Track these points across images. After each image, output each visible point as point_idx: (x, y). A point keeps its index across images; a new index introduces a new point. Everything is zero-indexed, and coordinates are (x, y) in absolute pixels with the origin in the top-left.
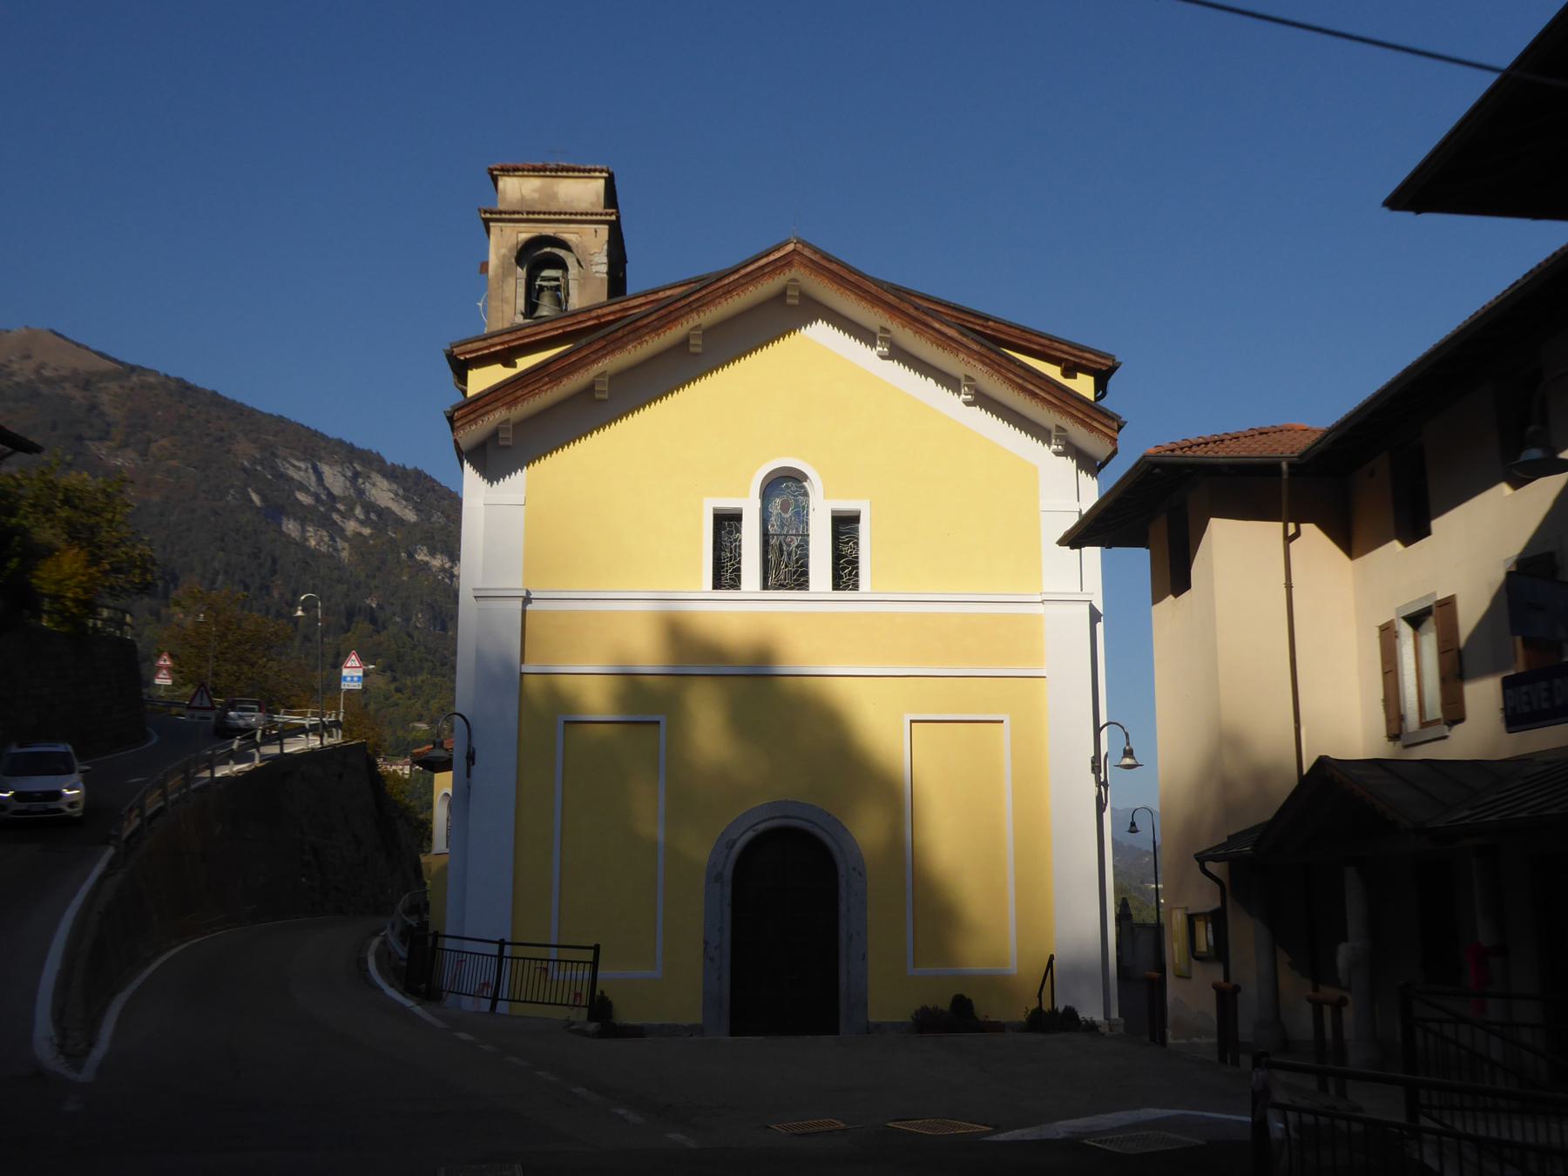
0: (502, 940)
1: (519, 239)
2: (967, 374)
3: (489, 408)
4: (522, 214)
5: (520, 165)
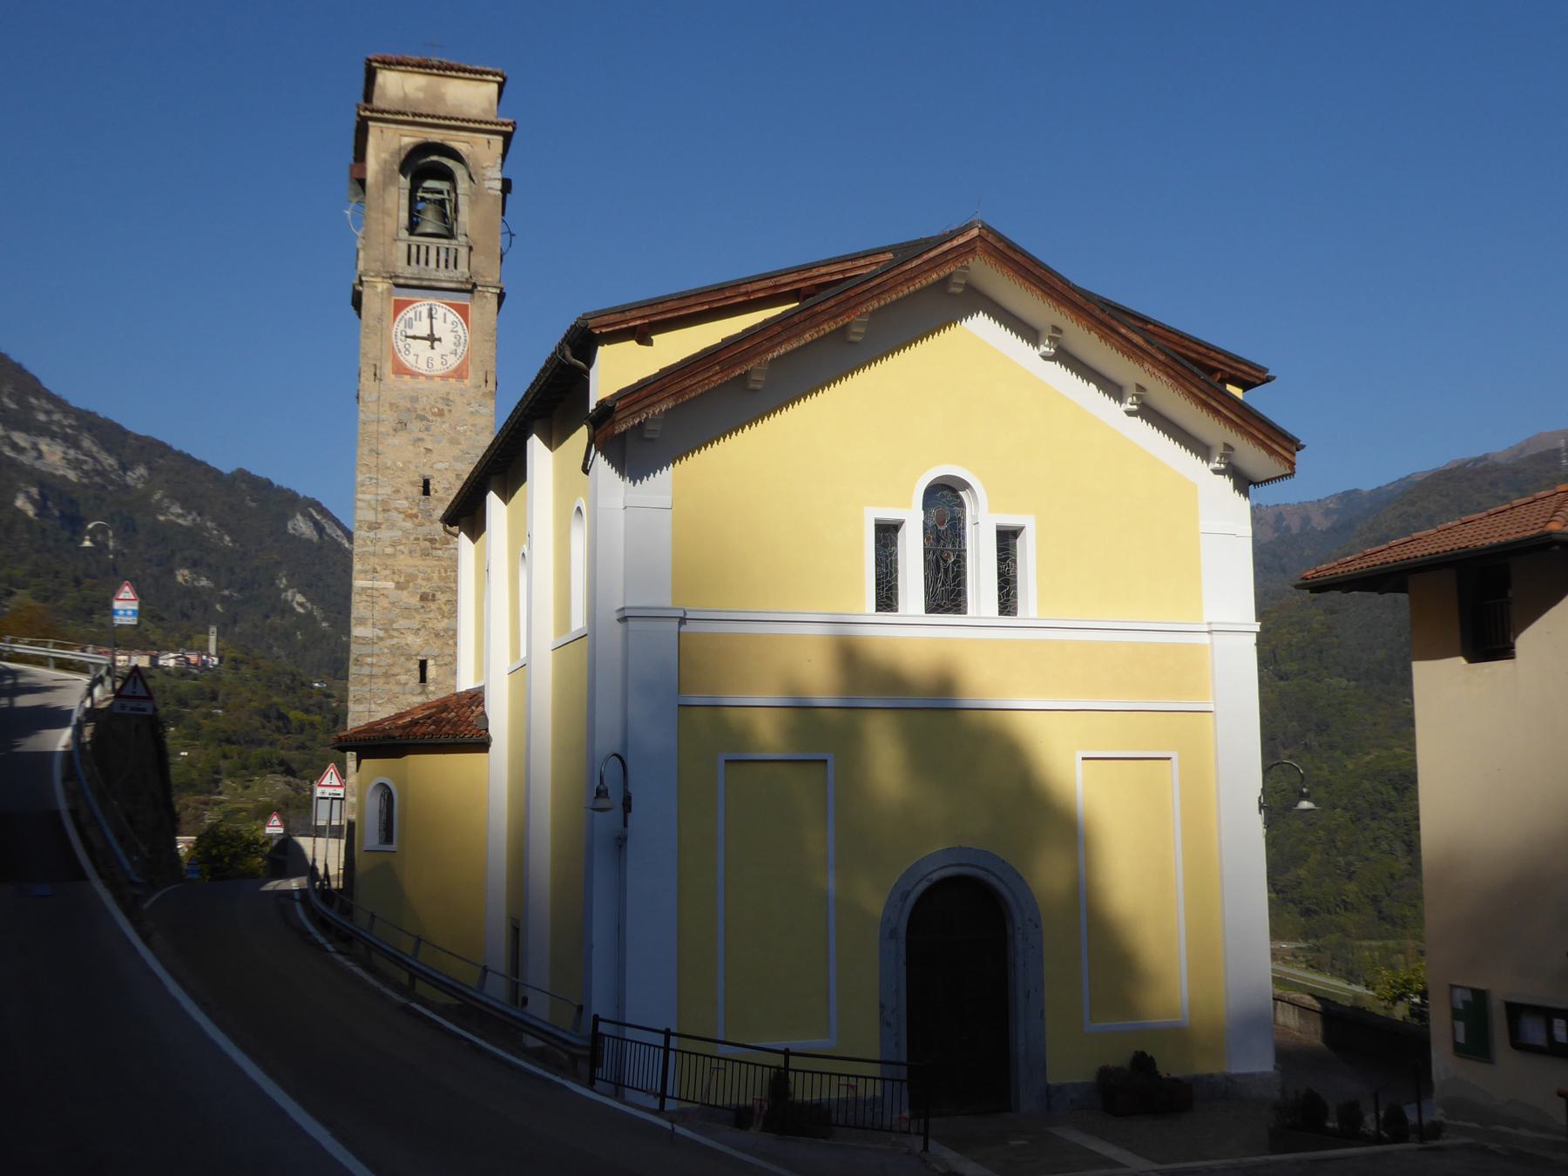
0: (787, 1050)
2: (1139, 383)
3: (654, 398)
4: (408, 115)
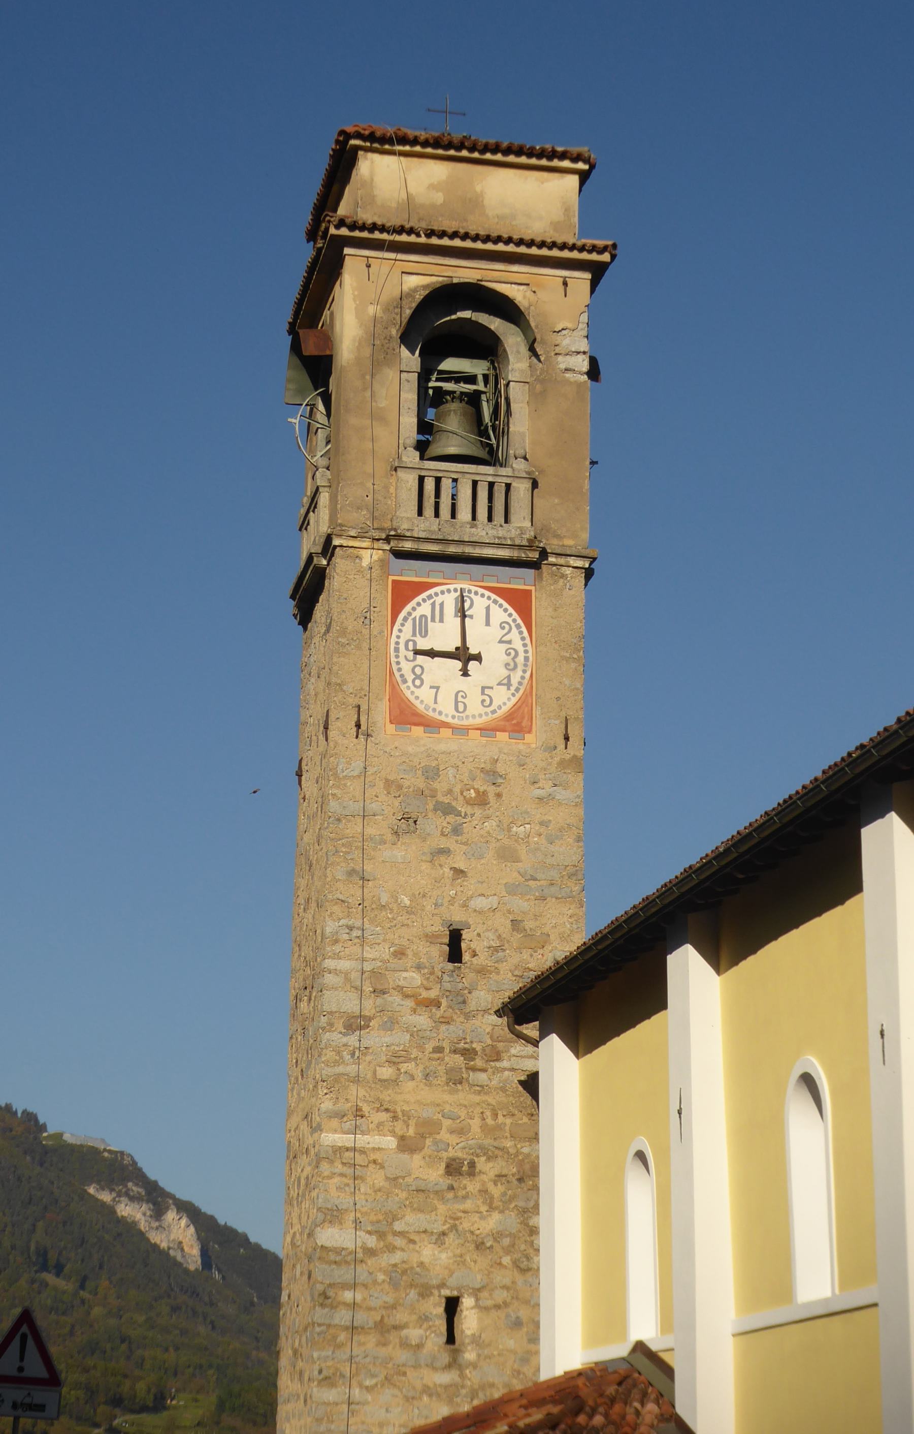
1: (405, 288)
4: (418, 235)
5: (411, 133)
